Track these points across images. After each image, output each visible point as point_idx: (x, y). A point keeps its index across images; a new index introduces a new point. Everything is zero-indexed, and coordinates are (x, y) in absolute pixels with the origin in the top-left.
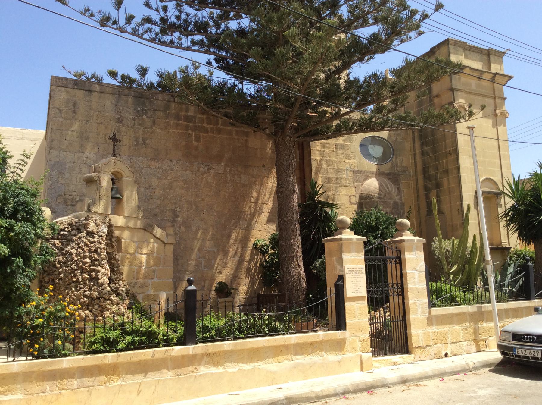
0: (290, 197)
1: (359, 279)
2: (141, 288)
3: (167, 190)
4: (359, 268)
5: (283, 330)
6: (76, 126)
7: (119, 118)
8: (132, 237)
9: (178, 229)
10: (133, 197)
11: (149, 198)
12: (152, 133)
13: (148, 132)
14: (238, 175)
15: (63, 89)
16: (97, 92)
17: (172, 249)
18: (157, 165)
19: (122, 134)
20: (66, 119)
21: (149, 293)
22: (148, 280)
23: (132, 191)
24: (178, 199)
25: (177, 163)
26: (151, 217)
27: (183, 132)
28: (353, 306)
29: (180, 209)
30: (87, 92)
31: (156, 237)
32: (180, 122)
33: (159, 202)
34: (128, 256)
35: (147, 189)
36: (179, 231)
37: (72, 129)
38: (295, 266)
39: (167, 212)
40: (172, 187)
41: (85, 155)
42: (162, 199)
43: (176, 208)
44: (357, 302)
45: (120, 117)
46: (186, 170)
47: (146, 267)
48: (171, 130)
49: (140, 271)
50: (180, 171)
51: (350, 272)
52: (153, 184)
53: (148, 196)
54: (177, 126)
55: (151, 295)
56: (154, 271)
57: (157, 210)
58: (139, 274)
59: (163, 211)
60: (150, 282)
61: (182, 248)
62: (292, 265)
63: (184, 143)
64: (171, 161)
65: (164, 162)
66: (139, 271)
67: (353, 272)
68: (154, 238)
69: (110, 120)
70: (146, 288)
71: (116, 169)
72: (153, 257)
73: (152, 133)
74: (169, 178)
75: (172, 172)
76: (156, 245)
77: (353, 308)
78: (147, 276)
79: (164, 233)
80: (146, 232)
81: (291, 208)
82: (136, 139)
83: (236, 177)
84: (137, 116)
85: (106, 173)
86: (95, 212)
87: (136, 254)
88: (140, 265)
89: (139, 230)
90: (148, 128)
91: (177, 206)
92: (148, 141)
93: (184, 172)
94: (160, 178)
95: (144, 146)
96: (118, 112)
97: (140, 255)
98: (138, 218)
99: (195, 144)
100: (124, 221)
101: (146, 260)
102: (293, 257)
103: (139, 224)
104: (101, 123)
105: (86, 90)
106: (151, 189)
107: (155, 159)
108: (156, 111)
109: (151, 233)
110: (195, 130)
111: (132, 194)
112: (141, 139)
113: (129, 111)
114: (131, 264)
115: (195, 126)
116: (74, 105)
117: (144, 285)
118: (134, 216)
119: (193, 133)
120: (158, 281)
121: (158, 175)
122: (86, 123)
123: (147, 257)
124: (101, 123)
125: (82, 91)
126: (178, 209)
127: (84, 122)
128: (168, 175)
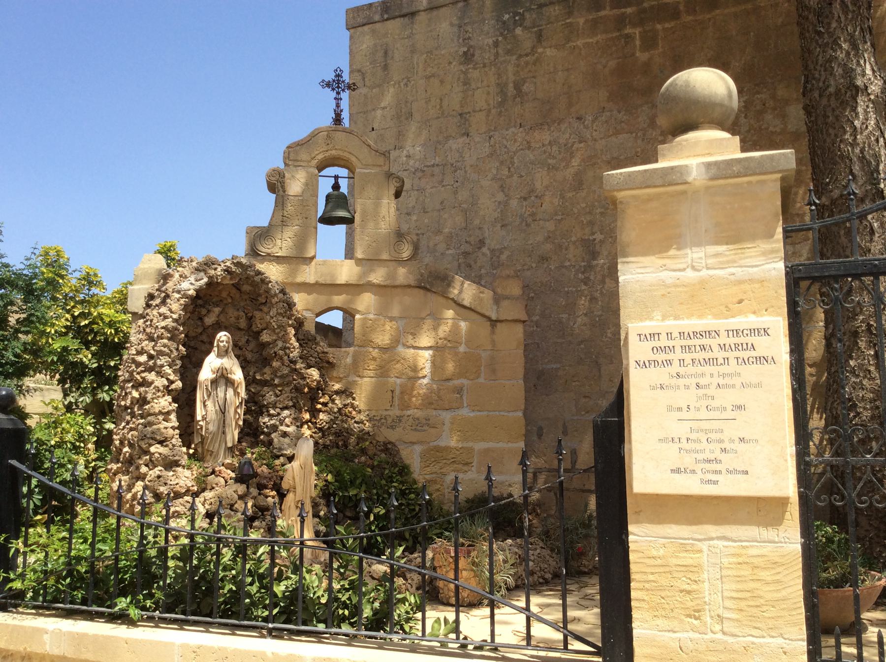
0: (837, 118)
1: (728, 398)
2: (416, 430)
3: (570, 195)
4: (737, 332)
5: (332, 619)
6: (388, 98)
7: (465, 53)
8: (383, 311)
9: (599, 287)
10: (384, 211)
11: (530, 220)
12: (534, 64)
13: (527, 63)
14: (774, 109)
15: (366, 28)
16: (424, 11)
17: (521, 335)
18: (546, 136)
19: (473, 86)
20: (372, 88)
21: (442, 443)
22: (440, 412)
23: (379, 198)
24: (598, 211)
25: (593, 121)
26: (534, 265)
27: (610, 36)
28: (684, 548)
29: (601, 237)
30: (406, 19)
31: (458, 305)
32: (602, 13)
33: (550, 226)
34: (375, 353)
35: (525, 199)
36: (602, 293)
37: (382, 105)
38: (861, 366)
39: (572, 247)
40: (581, 183)
41: (405, 152)
42: (559, 217)
43: (593, 234)
44: (712, 530)
45: (468, 50)
46: (617, 133)
47: (432, 379)
48: (580, 43)
49: (413, 389)
50: (601, 139)
51: (661, 357)
52: (539, 186)
53: (526, 215)
54: (594, 25)
55: (447, 449)
56: (459, 390)
57: (548, 246)
58: (411, 396)
59: (560, 246)
60: (446, 416)
61: (609, 335)
62: (852, 363)
63: (612, 64)
64: (579, 118)
65: (563, 127)
66: (407, 390)
67: (688, 357)
68: (458, 308)
69: (450, 63)
70: (433, 430)
71: (334, 152)
72: (456, 354)
73: (534, 64)
74: (575, 162)
75: (582, 145)
76: (463, 325)
77: (688, 559)
78: (432, 401)
79: (488, 294)
80: (429, 294)
81: (842, 157)
82: (502, 88)
83: (769, 117)
84: (502, 34)
85: (302, 164)
86: (269, 255)
87: (400, 349)
88: (411, 374)
89: (409, 290)
90: (527, 55)
91: (596, 229)
92: (527, 84)
93: (614, 139)
94: (552, 168)
95: (518, 99)
96: (464, 40)
97: (412, 351)
98: (400, 262)
99: (642, 57)
100: (356, 270)
101: (433, 363)
102: (855, 334)
103: (402, 274)
104: (433, 76)
105: (404, 16)
106: (533, 198)
107: (542, 124)
108: (544, 9)
109: (444, 295)
110: (641, 22)
111: (377, 205)
112: (511, 85)
113: (486, 28)
114: (383, 372)
115: (644, 11)
116: (386, 53)
117: (421, 425)
118: (385, 256)
119: (637, 31)
120: (472, 415)
121: (550, 161)
122: (406, 85)
123: (434, 356)
124: (433, 76)
125: (398, 19)
126: (599, 237)
127: (402, 84)
128: (572, 156)
